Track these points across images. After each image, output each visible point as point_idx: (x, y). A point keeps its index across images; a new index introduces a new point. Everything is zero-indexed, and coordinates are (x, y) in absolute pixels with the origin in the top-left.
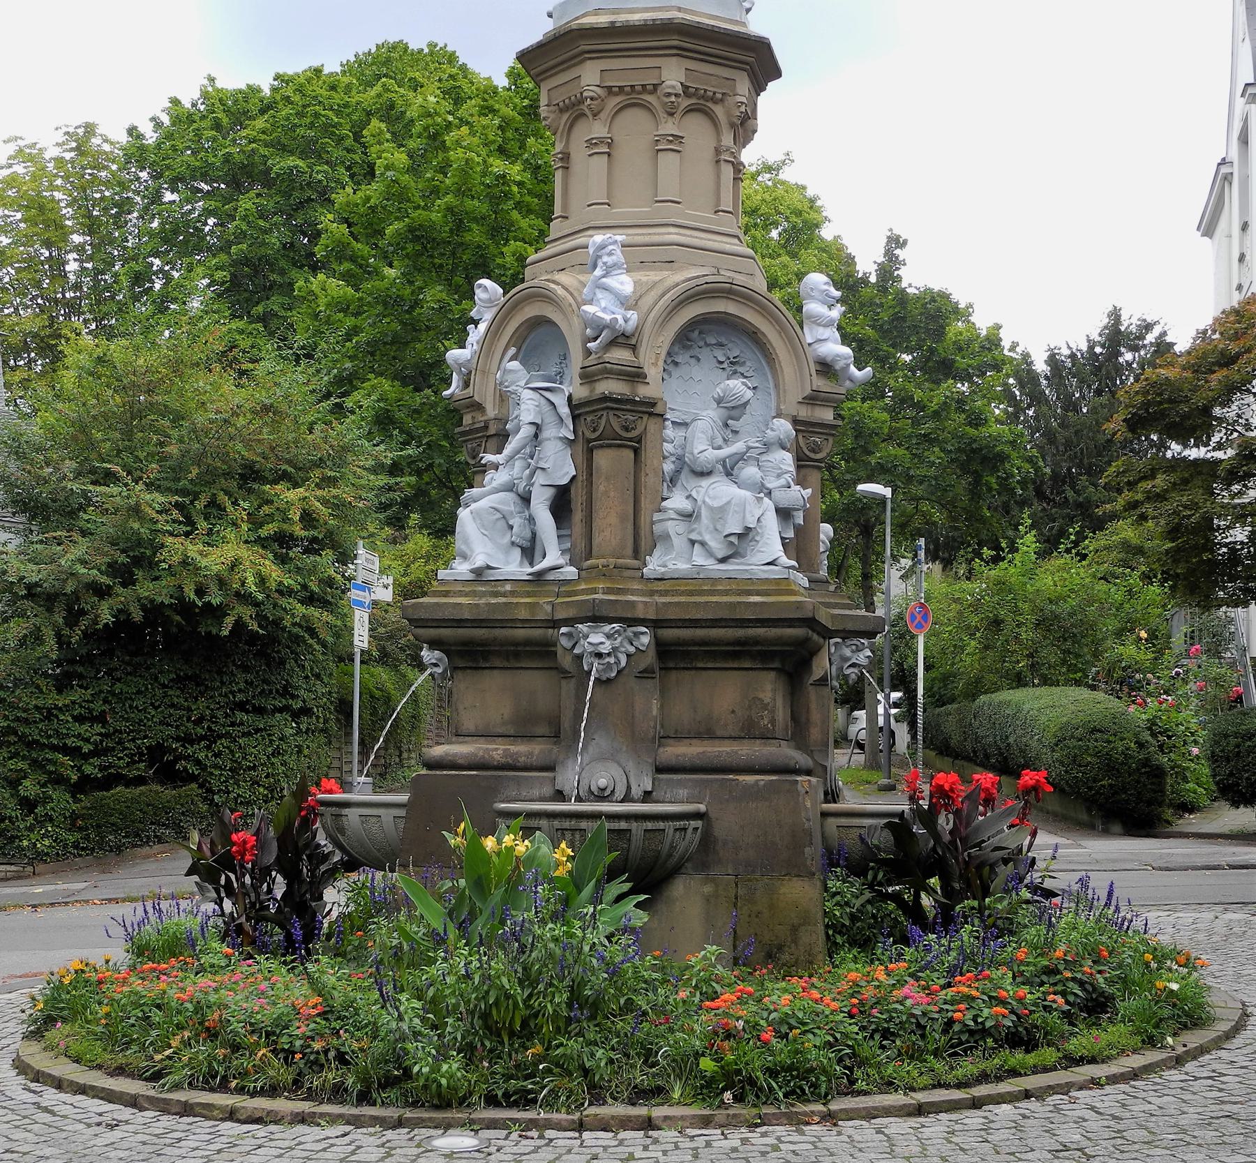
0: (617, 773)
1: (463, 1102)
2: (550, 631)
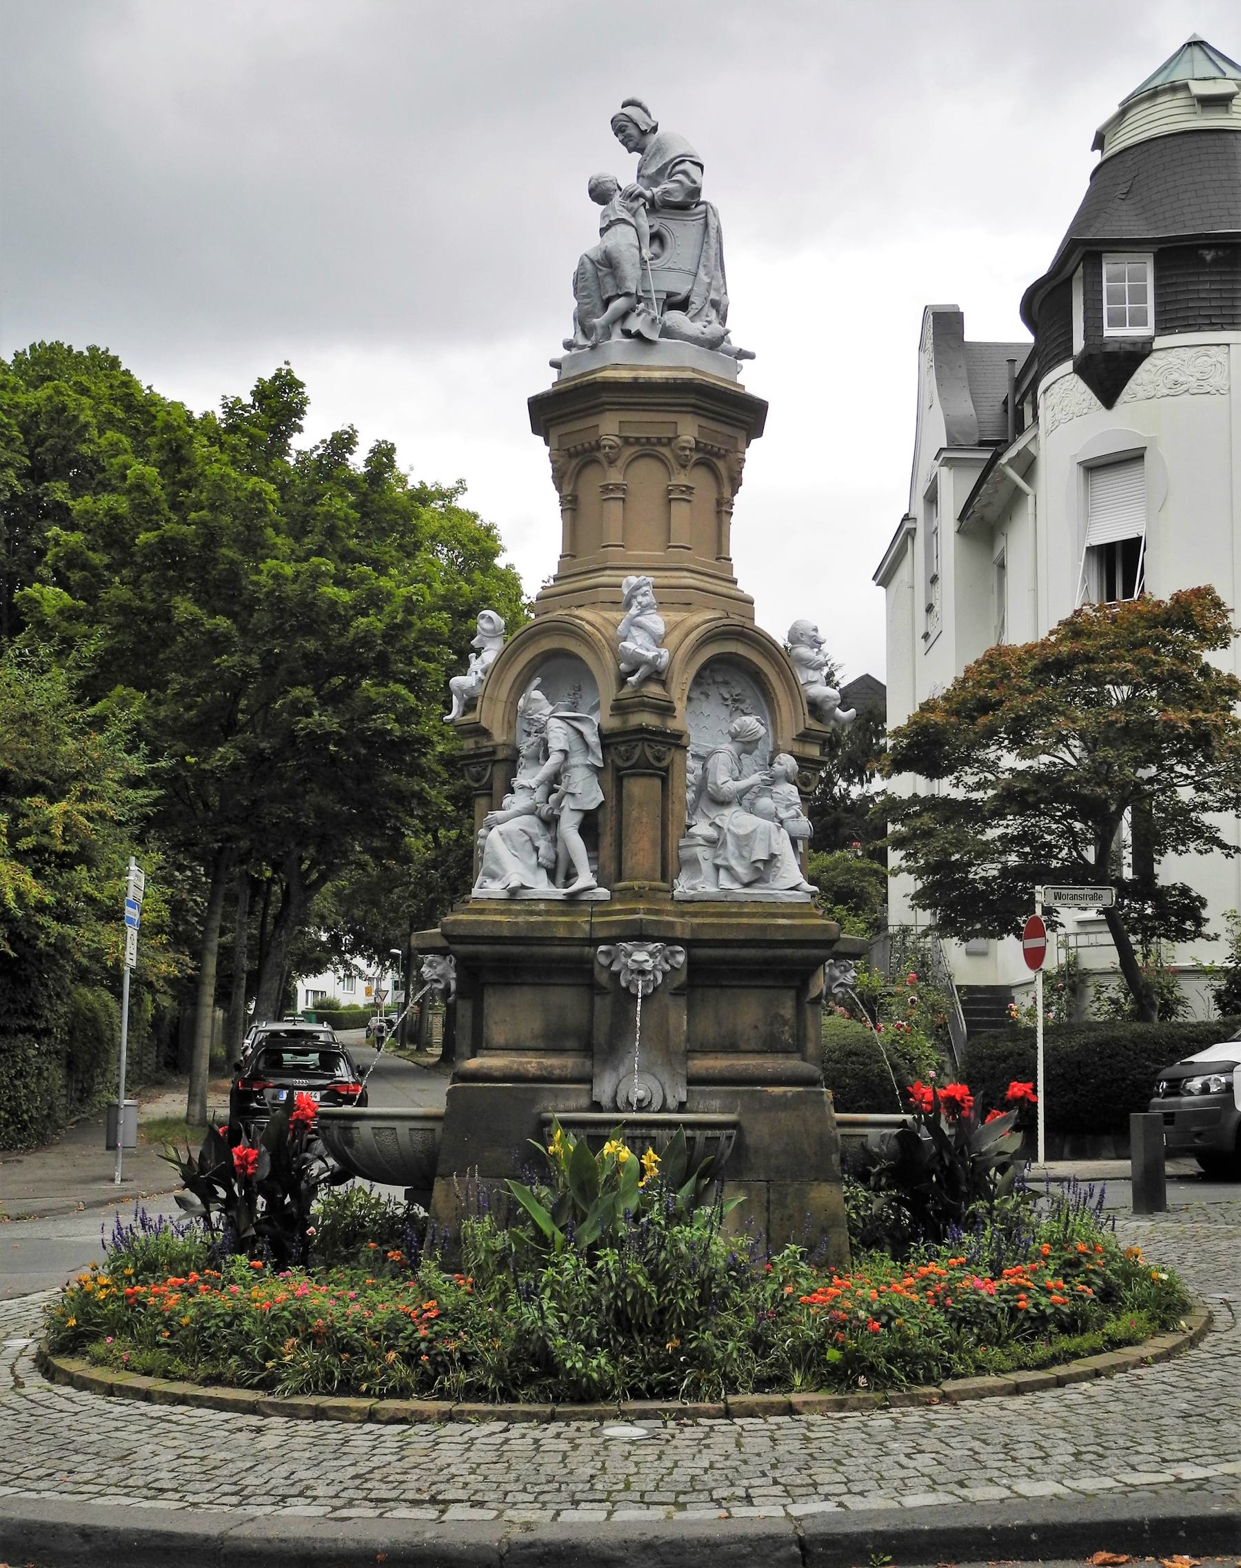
0: (655, 1086)
1: (606, 1396)
2: (587, 949)
